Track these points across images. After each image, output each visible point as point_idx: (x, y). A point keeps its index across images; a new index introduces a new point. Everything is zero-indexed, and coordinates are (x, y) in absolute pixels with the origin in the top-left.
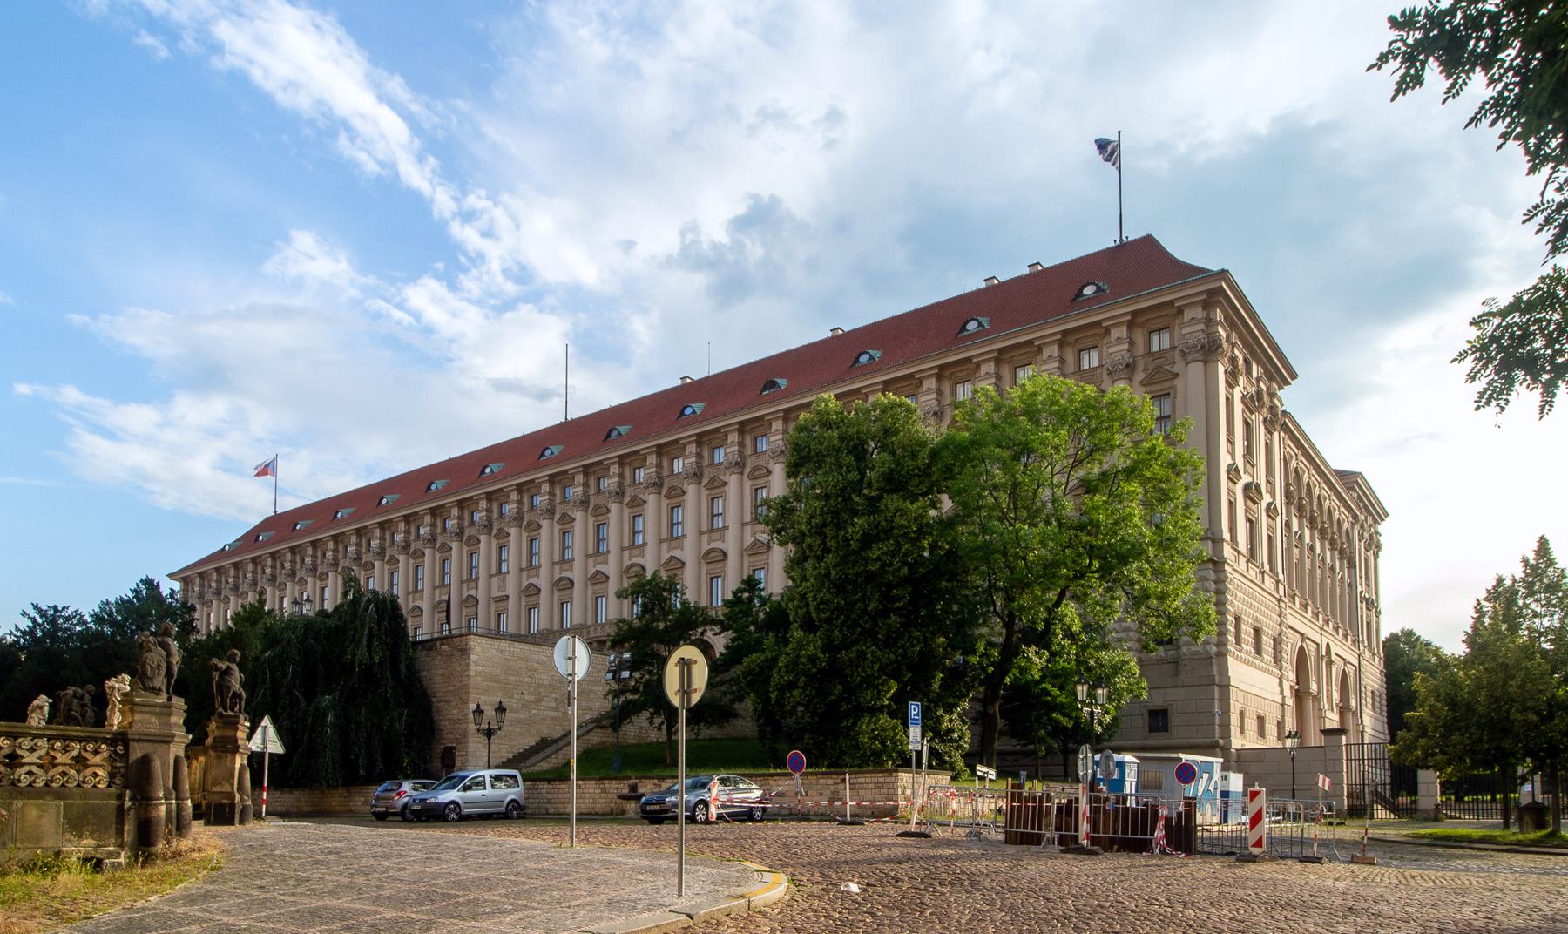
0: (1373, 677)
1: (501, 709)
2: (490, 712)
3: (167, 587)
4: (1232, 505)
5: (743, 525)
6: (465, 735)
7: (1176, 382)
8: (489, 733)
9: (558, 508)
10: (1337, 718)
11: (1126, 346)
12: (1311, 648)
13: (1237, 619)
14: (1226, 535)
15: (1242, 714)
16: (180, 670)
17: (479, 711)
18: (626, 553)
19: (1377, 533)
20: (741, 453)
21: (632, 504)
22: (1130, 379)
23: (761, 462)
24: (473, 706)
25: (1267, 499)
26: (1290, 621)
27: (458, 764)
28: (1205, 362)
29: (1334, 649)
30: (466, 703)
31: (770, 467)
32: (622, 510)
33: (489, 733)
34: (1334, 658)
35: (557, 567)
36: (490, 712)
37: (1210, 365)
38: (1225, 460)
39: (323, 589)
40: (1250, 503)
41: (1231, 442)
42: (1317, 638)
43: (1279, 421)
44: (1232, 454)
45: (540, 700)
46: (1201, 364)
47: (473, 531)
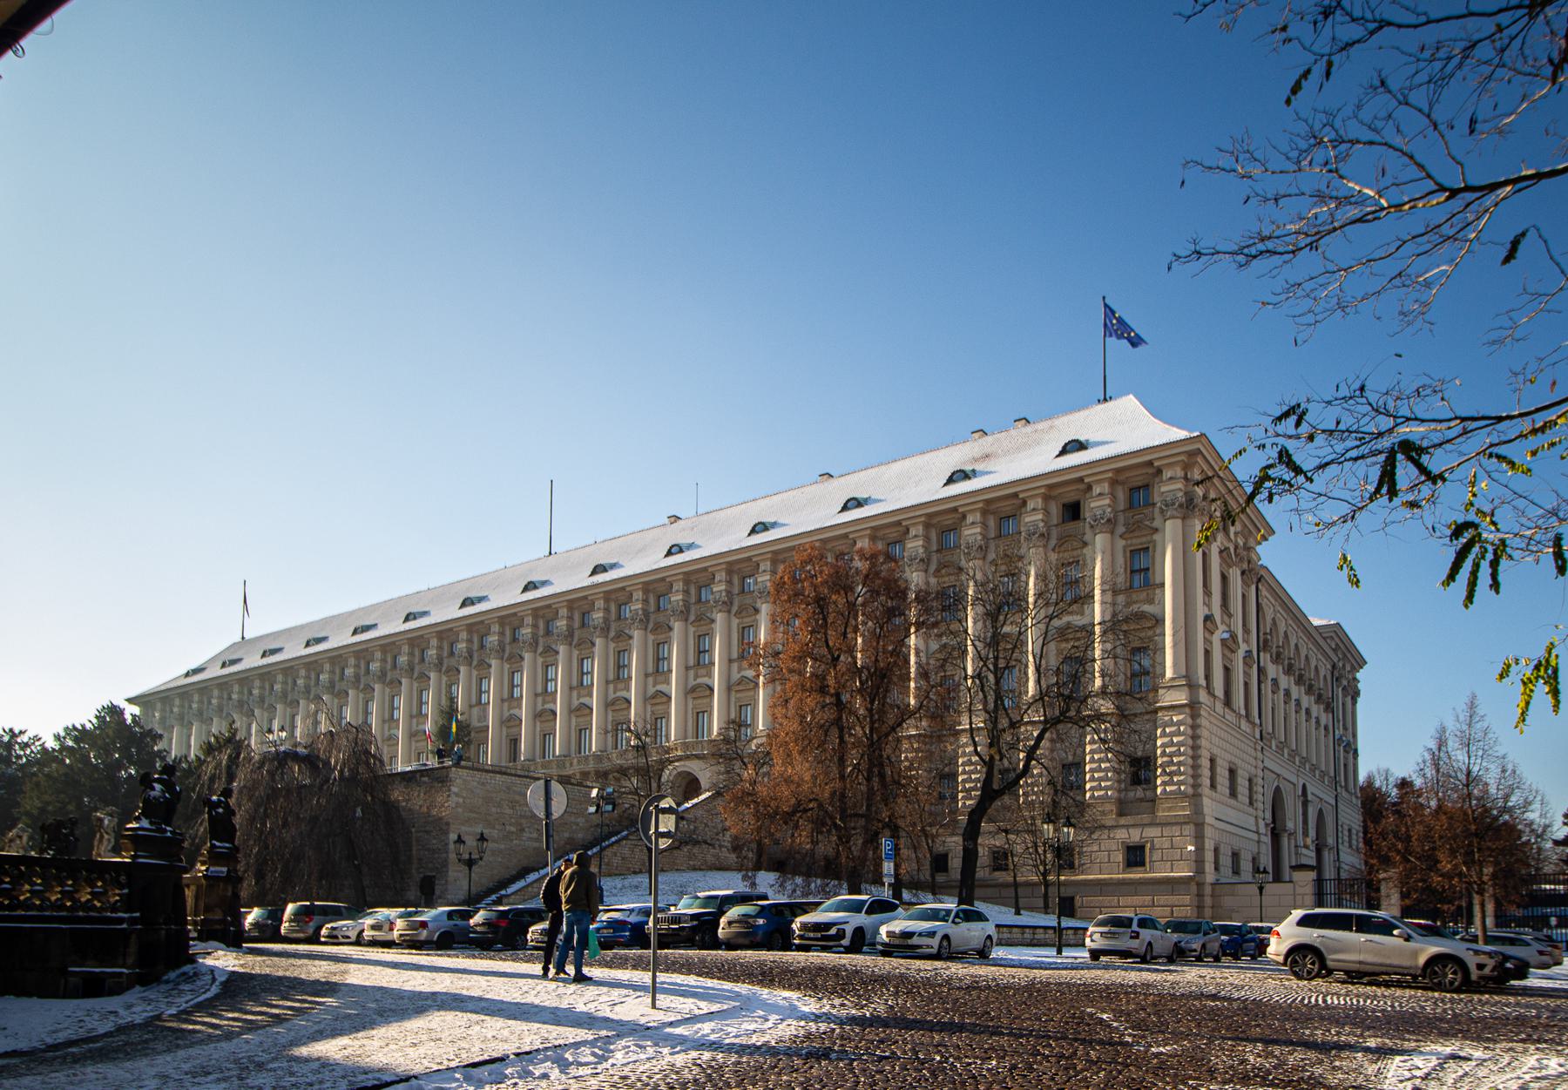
0: (1352, 817)
1: (482, 838)
2: (471, 842)
3: (131, 711)
4: (1207, 653)
5: (730, 661)
6: (445, 864)
7: (1156, 537)
8: (470, 863)
9: (541, 641)
10: (1313, 854)
11: (1107, 501)
12: (1284, 786)
13: (1212, 761)
14: (1203, 682)
15: (1216, 850)
16: (324, 1064)
17: (460, 840)
18: (735, 666)
19: (1355, 679)
20: (729, 592)
21: (699, 619)
22: (984, 558)
23: (748, 601)
24: (453, 837)
25: (1243, 647)
26: (1268, 763)
27: (437, 892)
28: (1184, 519)
29: (1310, 789)
30: (447, 833)
31: (758, 605)
32: (607, 647)
33: (470, 863)
34: (1310, 797)
35: (540, 699)
36: (471, 842)
37: (1188, 522)
38: (1201, 612)
39: (293, 717)
40: (1227, 652)
41: (1207, 592)
42: (1294, 779)
43: (1257, 576)
44: (1208, 605)
45: (522, 830)
46: (1179, 522)
47: (453, 662)
